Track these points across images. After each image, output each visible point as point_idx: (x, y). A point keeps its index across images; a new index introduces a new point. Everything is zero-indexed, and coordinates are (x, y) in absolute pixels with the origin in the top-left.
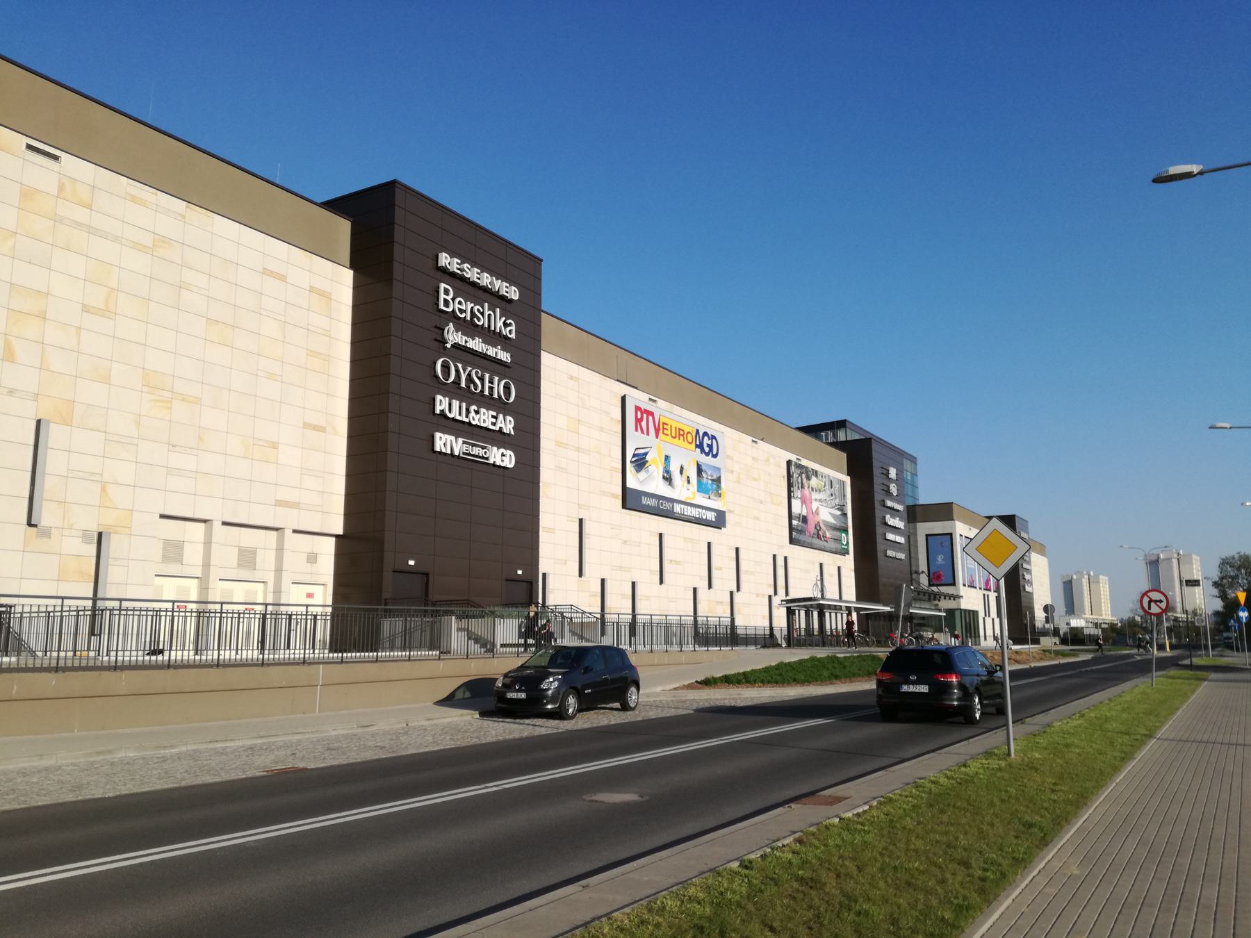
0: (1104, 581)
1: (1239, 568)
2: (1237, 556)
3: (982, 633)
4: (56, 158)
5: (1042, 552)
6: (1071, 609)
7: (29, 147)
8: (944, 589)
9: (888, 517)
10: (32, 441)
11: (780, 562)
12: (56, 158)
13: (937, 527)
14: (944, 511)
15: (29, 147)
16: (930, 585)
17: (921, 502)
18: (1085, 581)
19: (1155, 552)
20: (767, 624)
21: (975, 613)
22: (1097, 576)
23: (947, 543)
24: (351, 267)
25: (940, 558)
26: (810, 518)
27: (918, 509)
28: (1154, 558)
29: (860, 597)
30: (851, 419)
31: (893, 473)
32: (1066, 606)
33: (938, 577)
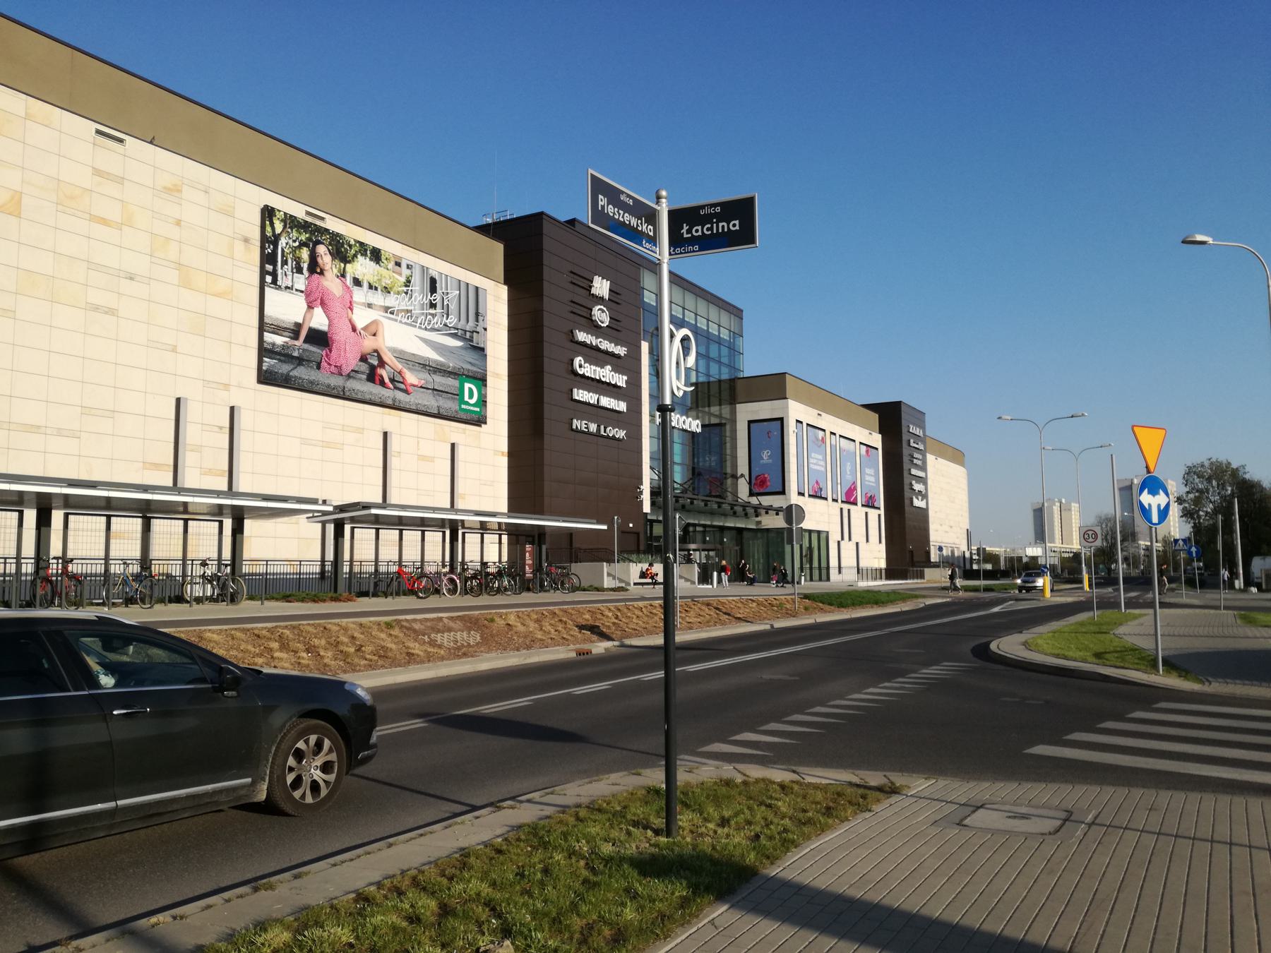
0: (1075, 506)
1: (1209, 480)
2: (1207, 464)
3: (833, 562)
4: (121, 141)
5: (957, 456)
6: (1040, 536)
7: (98, 132)
8: (766, 501)
9: (578, 360)
10: (173, 416)
11: (845, 514)
12: (121, 141)
13: (763, 410)
14: (774, 386)
15: (98, 132)
16: (751, 494)
17: (747, 373)
18: (1056, 508)
19: (1129, 477)
20: (419, 558)
21: (822, 536)
22: (1069, 503)
23: (777, 433)
24: (505, 283)
25: (766, 455)
26: (342, 335)
27: (739, 385)
28: (1128, 483)
29: (518, 502)
30: (579, 218)
31: (601, 287)
32: (1036, 533)
33: (763, 482)
